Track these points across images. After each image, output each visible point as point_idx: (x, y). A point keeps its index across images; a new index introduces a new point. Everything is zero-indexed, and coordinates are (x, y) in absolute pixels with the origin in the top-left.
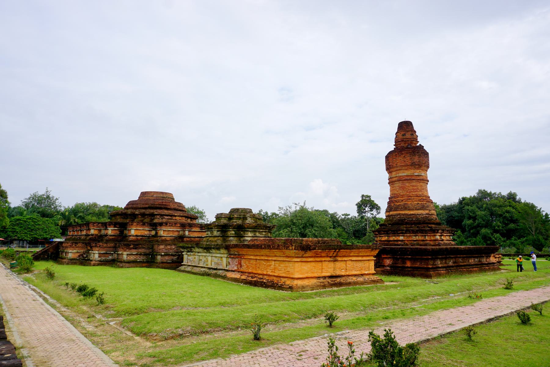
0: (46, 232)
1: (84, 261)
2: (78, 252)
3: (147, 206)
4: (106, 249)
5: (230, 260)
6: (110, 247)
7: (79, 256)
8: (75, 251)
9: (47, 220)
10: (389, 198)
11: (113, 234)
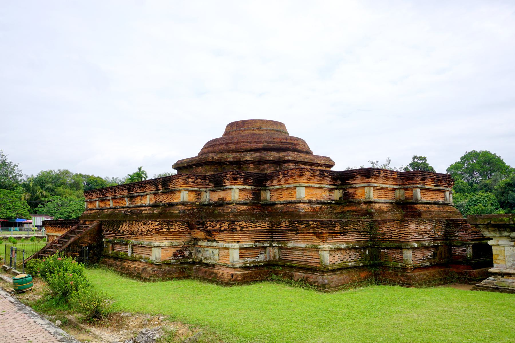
0: (10, 209)
1: (186, 267)
2: (172, 246)
3: (260, 146)
4: (253, 235)
5: (331, 253)
6: (261, 232)
7: (175, 255)
8: (166, 243)
9: (10, 193)
10: (462, 158)
11: (241, 200)
